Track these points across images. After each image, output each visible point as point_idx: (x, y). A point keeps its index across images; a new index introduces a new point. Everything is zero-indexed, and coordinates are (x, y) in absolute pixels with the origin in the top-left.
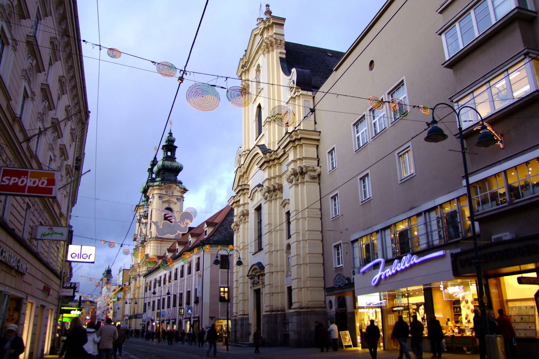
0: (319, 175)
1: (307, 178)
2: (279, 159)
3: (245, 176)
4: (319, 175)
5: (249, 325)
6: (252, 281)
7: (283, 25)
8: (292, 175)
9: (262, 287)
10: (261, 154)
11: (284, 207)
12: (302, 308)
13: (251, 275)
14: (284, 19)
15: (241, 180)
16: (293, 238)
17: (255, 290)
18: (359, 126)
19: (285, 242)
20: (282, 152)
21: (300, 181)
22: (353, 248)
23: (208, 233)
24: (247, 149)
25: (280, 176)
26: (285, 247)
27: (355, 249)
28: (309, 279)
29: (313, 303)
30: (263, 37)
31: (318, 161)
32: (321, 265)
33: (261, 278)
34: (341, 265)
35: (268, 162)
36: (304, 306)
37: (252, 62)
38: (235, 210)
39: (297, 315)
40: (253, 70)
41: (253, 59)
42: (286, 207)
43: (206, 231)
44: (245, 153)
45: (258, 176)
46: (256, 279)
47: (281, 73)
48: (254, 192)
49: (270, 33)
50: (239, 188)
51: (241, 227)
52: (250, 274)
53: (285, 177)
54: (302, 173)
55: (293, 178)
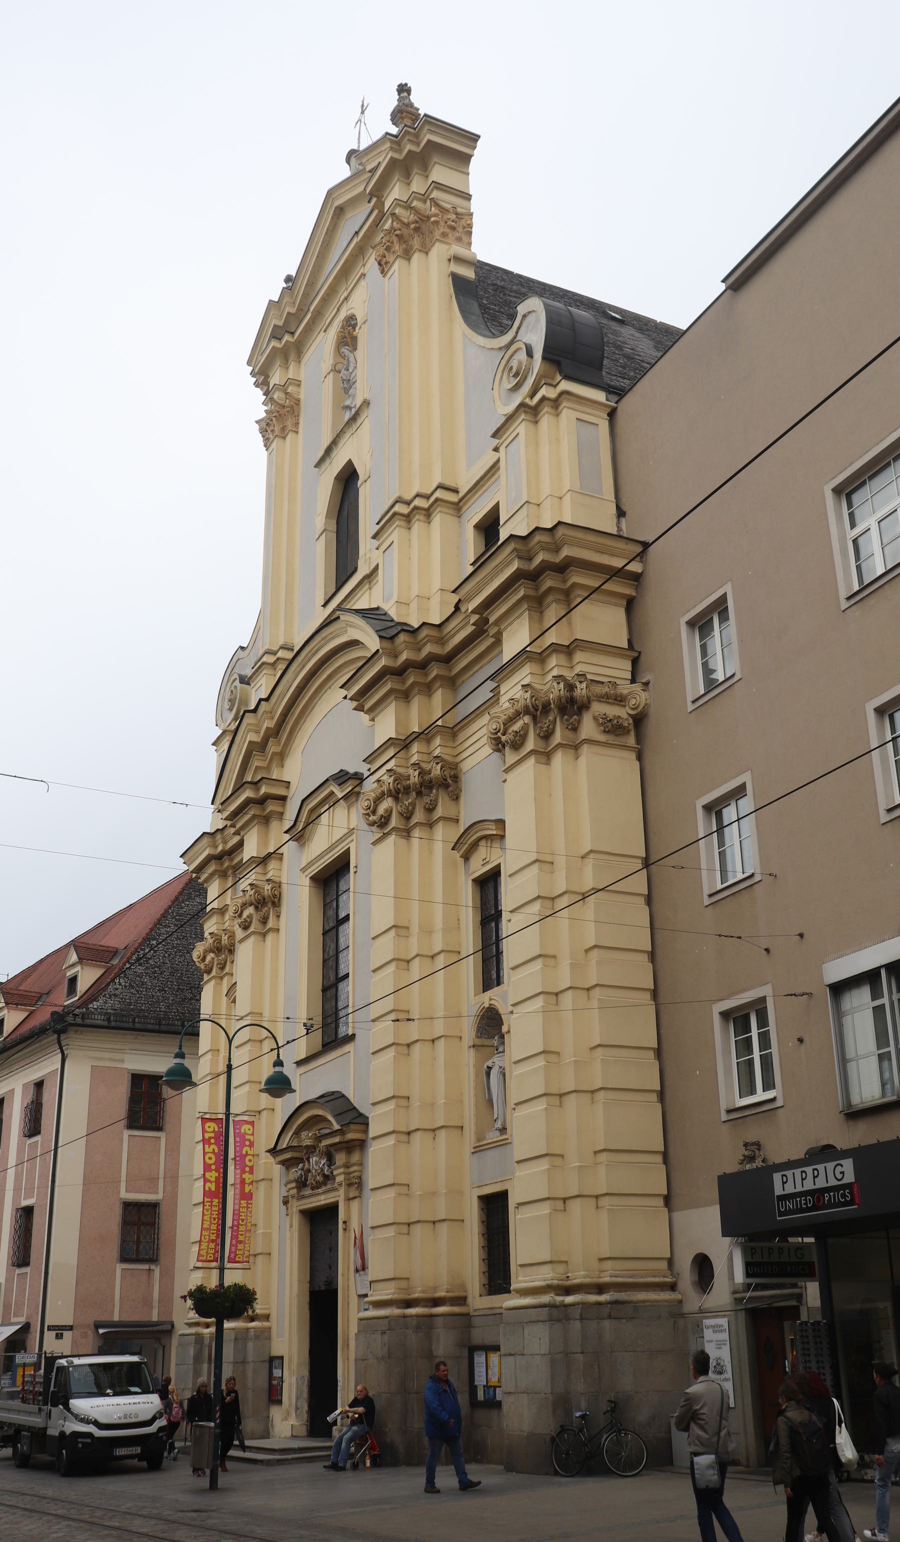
0: (639, 720)
1: (588, 727)
2: (447, 659)
3: (273, 748)
4: (639, 720)
5: (275, 1361)
6: (295, 1173)
7: (466, 159)
8: (211, 951)
9: (349, 1199)
10: (372, 643)
11: (466, 857)
12: (568, 1290)
13: (289, 1148)
14: (473, 139)
15: (256, 762)
16: (518, 982)
17: (305, 1213)
18: (857, 498)
19: (473, 1001)
20: (469, 629)
21: (557, 738)
22: (839, 1015)
23: (82, 986)
24: (281, 642)
25: (453, 732)
26: (468, 1028)
27: (847, 1021)
28: (603, 1157)
29: (620, 1265)
30: (380, 204)
31: (635, 662)
32: (654, 1097)
33: (340, 1158)
34: (761, 1095)
35: (399, 672)
36: (579, 1277)
37: (318, 314)
38: (213, 890)
39: (551, 1319)
40: (323, 346)
41: (327, 299)
42: (482, 851)
43: (73, 981)
44: (270, 659)
45: (338, 736)
46: (316, 1163)
47: (460, 325)
48: (317, 805)
49: (418, 185)
50: (248, 793)
51: (245, 952)
52: (284, 1144)
53: (480, 733)
54: (571, 707)
55: (525, 727)
